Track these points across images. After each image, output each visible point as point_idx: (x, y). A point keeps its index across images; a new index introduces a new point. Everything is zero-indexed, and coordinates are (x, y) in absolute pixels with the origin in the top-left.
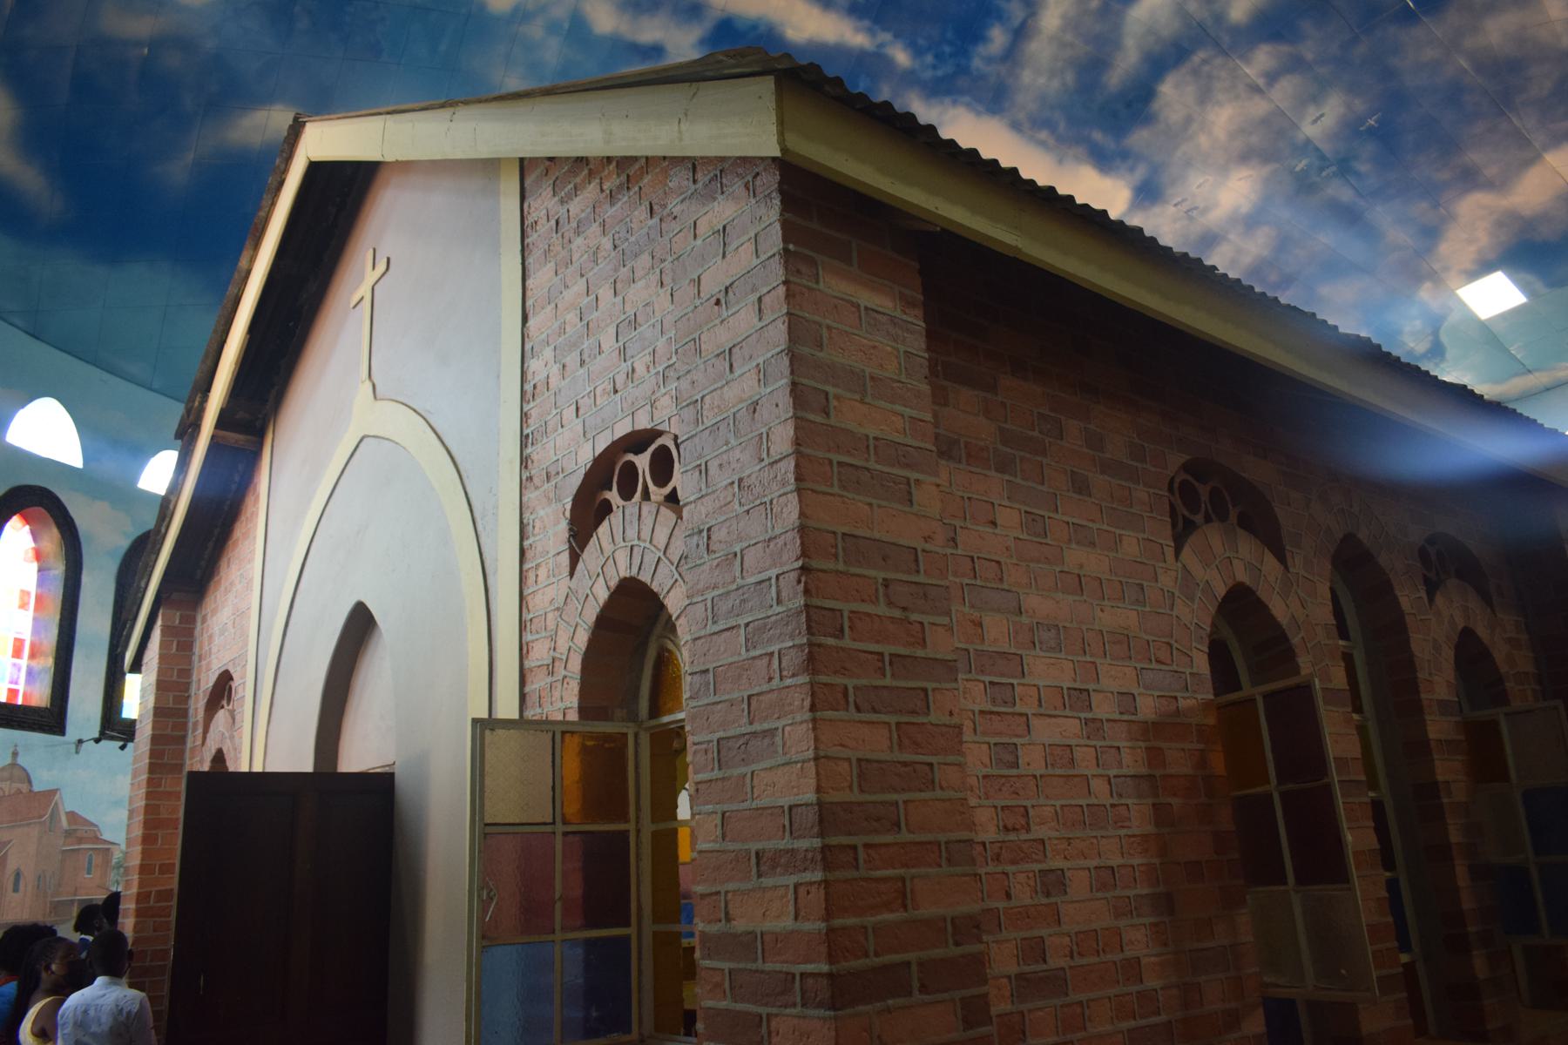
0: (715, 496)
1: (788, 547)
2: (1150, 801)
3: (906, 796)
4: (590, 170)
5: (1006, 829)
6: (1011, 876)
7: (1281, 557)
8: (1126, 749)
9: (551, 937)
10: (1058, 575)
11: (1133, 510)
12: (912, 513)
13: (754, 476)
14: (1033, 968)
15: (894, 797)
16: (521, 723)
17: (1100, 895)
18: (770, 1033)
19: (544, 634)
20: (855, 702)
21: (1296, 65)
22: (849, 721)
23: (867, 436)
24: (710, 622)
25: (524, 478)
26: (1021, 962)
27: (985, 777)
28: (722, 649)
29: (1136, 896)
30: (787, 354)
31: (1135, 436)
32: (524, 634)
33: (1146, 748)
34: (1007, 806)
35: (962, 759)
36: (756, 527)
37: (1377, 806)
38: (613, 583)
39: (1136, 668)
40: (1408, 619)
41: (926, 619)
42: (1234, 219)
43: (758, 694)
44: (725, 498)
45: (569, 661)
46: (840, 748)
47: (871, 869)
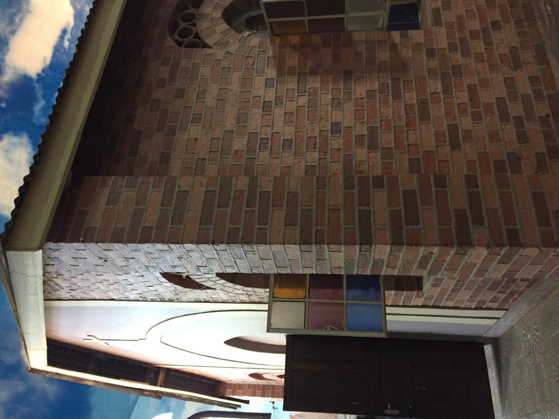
3: (299, 205)
4: (48, 280)
10: (217, 111)
11: (191, 67)
12: (192, 190)
15: (299, 211)
16: (270, 304)
23: (161, 209)
25: (177, 301)
26: (364, 147)
27: (295, 156)
31: (159, 61)
38: (218, 278)
39: (256, 76)
43: (260, 256)
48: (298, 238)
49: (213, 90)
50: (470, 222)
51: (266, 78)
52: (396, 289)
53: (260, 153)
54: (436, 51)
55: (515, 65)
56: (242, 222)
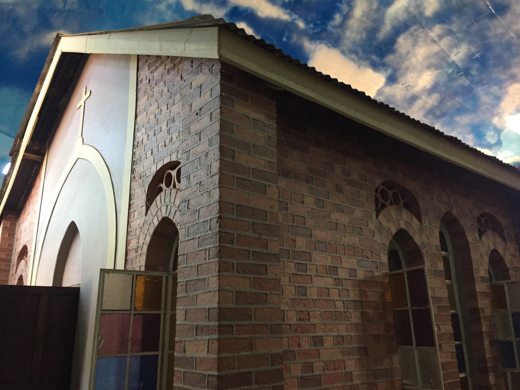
0: (191, 188)
1: (215, 208)
2: (360, 311)
4: (162, 61)
5: (300, 319)
6: (301, 338)
7: (420, 220)
8: (351, 290)
9: (125, 355)
11: (360, 199)
12: (267, 198)
13: (205, 181)
15: (250, 306)
16: (125, 271)
17: (337, 346)
19: (135, 237)
20: (237, 269)
21: (450, 33)
23: (249, 168)
25: (132, 177)
27: (292, 299)
29: (352, 348)
30: (219, 135)
32: (128, 236)
33: (359, 290)
34: (301, 311)
36: (204, 200)
37: (454, 318)
38: (160, 219)
39: (357, 259)
40: (470, 245)
41: (267, 238)
42: (424, 90)
43: (201, 264)
44: (195, 189)
45: (143, 248)
47: (238, 335)
48: (225, 306)
49: (343, 219)
51: (356, 269)
56: (238, 247)
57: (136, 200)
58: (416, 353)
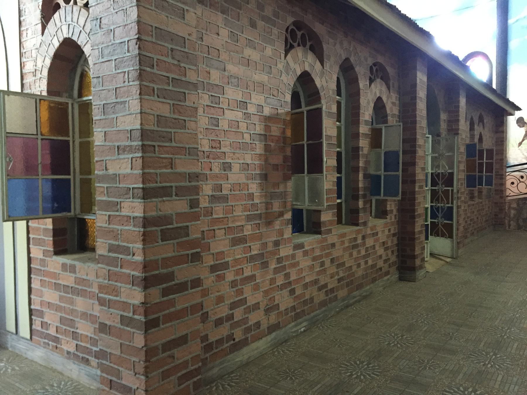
2: (264, 143)
5: (212, 147)
6: (212, 163)
7: (322, 64)
9: (37, 177)
14: (218, 193)
15: (170, 130)
16: (21, 94)
17: (243, 172)
18: (121, 208)
19: (31, 59)
22: (155, 101)
24: (101, 57)
27: (206, 129)
28: (105, 69)
32: (22, 58)
35: (196, 119)
36: (119, 19)
37: (339, 154)
38: (61, 39)
40: (361, 91)
41: (187, 66)
43: (119, 88)
44: (107, 5)
46: (150, 110)
48: (147, 127)
49: (254, 55)
50: (164, 285)
52: (54, 230)
53: (208, 96)
54: (278, 248)
55: (268, 309)
57: (27, 17)
58: (306, 179)
